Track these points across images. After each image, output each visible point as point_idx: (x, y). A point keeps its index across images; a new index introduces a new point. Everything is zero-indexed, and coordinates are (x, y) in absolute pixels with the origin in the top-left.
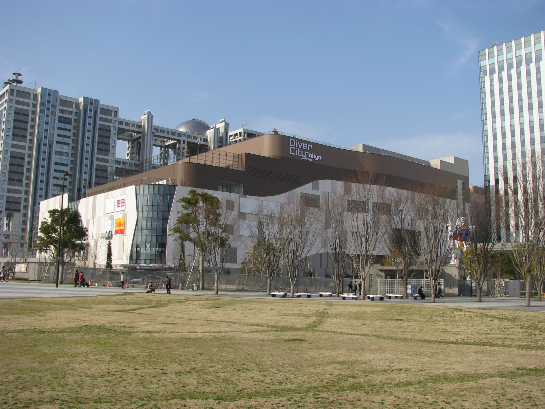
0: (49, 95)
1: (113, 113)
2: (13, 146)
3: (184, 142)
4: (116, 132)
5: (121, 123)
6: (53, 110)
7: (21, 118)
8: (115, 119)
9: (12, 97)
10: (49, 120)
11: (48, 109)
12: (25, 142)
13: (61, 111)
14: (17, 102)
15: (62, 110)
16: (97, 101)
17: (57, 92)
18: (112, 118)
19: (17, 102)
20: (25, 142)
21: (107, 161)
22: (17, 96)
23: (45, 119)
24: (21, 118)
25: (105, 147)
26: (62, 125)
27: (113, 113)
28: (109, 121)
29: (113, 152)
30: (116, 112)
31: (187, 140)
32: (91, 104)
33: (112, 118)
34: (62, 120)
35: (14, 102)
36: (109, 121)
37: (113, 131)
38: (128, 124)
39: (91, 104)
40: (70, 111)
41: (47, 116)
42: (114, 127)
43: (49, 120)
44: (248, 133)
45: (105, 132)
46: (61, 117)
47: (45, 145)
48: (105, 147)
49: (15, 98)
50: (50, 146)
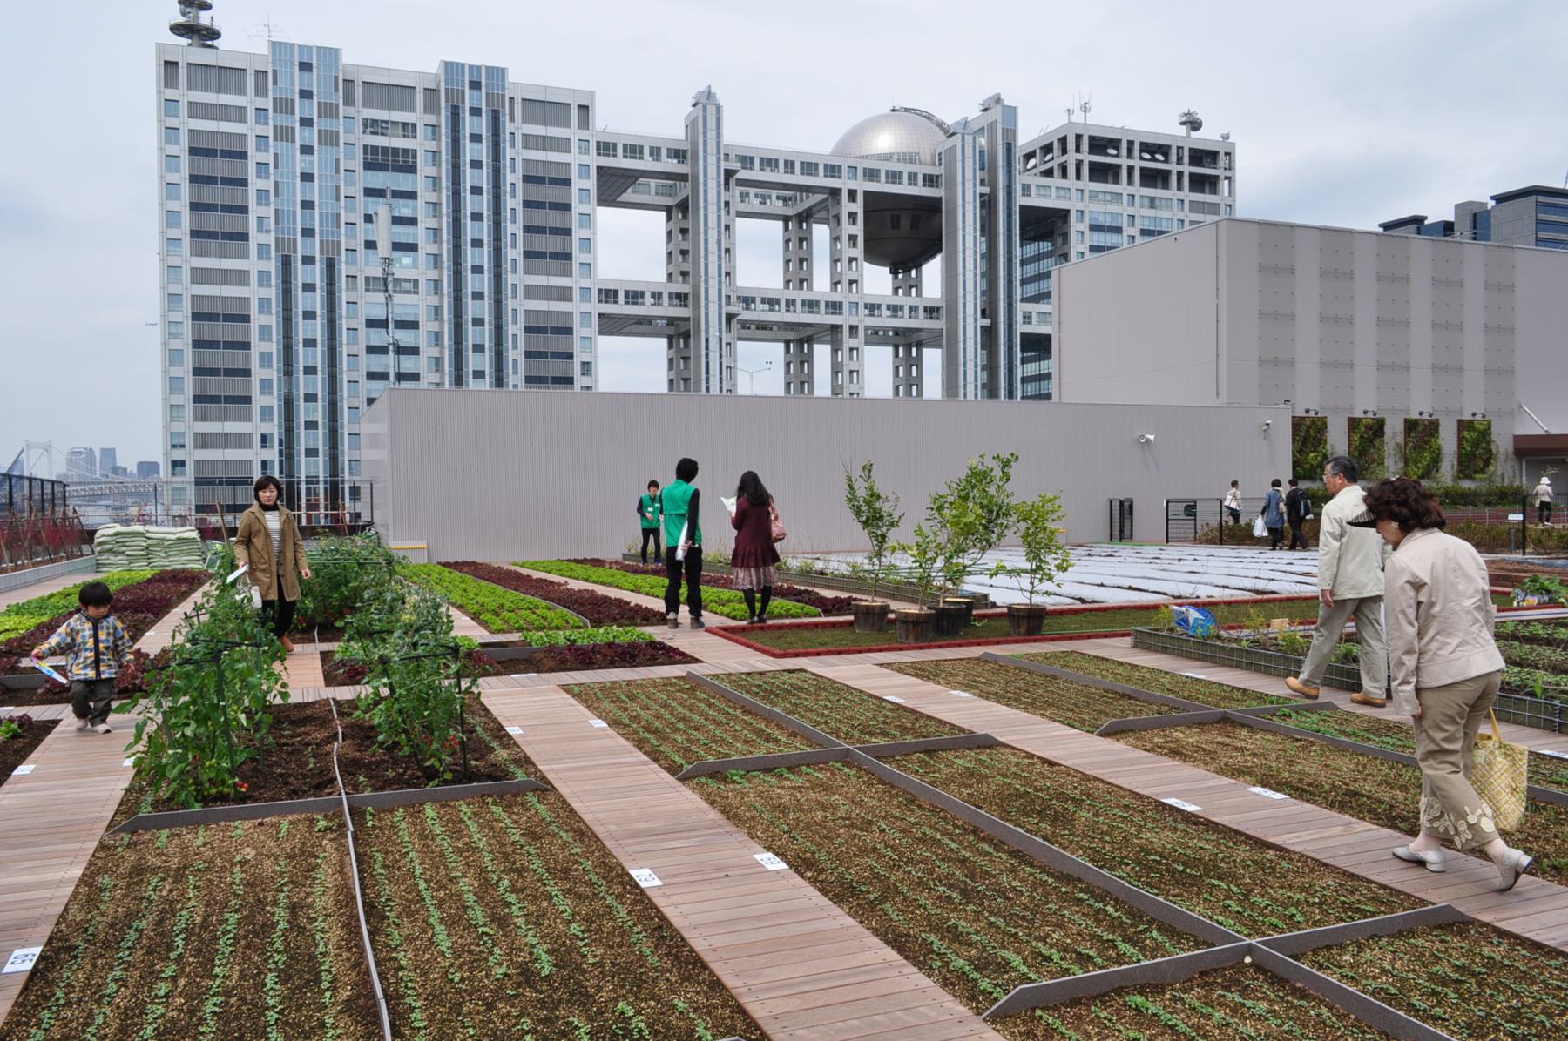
0: (306, 67)
1: (574, 112)
2: (199, 276)
3: (852, 195)
4: (591, 183)
5: (606, 148)
6: (328, 124)
7: (218, 167)
8: (583, 134)
9: (171, 94)
10: (315, 164)
11: (306, 122)
12: (245, 256)
13: (372, 126)
14: (197, 110)
15: (375, 122)
16: (498, 74)
17: (501, 72)
18: (573, 133)
19: (197, 110)
20: (245, 256)
21: (564, 294)
22: (367, 103)
23: (300, 163)
24: (218, 167)
25: (552, 245)
26: (379, 179)
27: (420, 98)
28: (563, 145)
29: (585, 258)
30: (584, 109)
31: (863, 186)
32: (475, 85)
33: (573, 133)
34: (376, 160)
35: (184, 109)
36: (563, 145)
37: (577, 183)
38: (634, 151)
39: (475, 85)
40: (405, 125)
41: (307, 150)
42: (581, 165)
43: (315, 164)
44: (1092, 139)
45: (548, 185)
46: (375, 149)
47: (308, 260)
48: (551, 244)
49: (185, 95)
50: (331, 265)
